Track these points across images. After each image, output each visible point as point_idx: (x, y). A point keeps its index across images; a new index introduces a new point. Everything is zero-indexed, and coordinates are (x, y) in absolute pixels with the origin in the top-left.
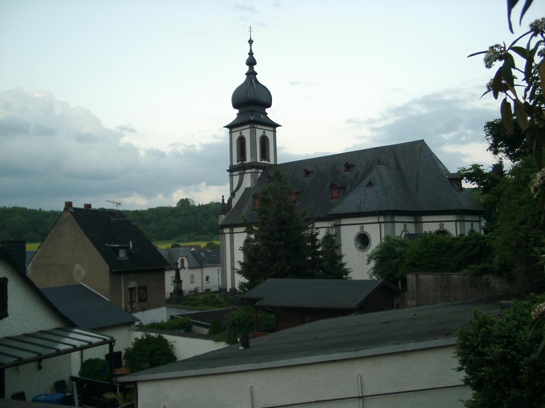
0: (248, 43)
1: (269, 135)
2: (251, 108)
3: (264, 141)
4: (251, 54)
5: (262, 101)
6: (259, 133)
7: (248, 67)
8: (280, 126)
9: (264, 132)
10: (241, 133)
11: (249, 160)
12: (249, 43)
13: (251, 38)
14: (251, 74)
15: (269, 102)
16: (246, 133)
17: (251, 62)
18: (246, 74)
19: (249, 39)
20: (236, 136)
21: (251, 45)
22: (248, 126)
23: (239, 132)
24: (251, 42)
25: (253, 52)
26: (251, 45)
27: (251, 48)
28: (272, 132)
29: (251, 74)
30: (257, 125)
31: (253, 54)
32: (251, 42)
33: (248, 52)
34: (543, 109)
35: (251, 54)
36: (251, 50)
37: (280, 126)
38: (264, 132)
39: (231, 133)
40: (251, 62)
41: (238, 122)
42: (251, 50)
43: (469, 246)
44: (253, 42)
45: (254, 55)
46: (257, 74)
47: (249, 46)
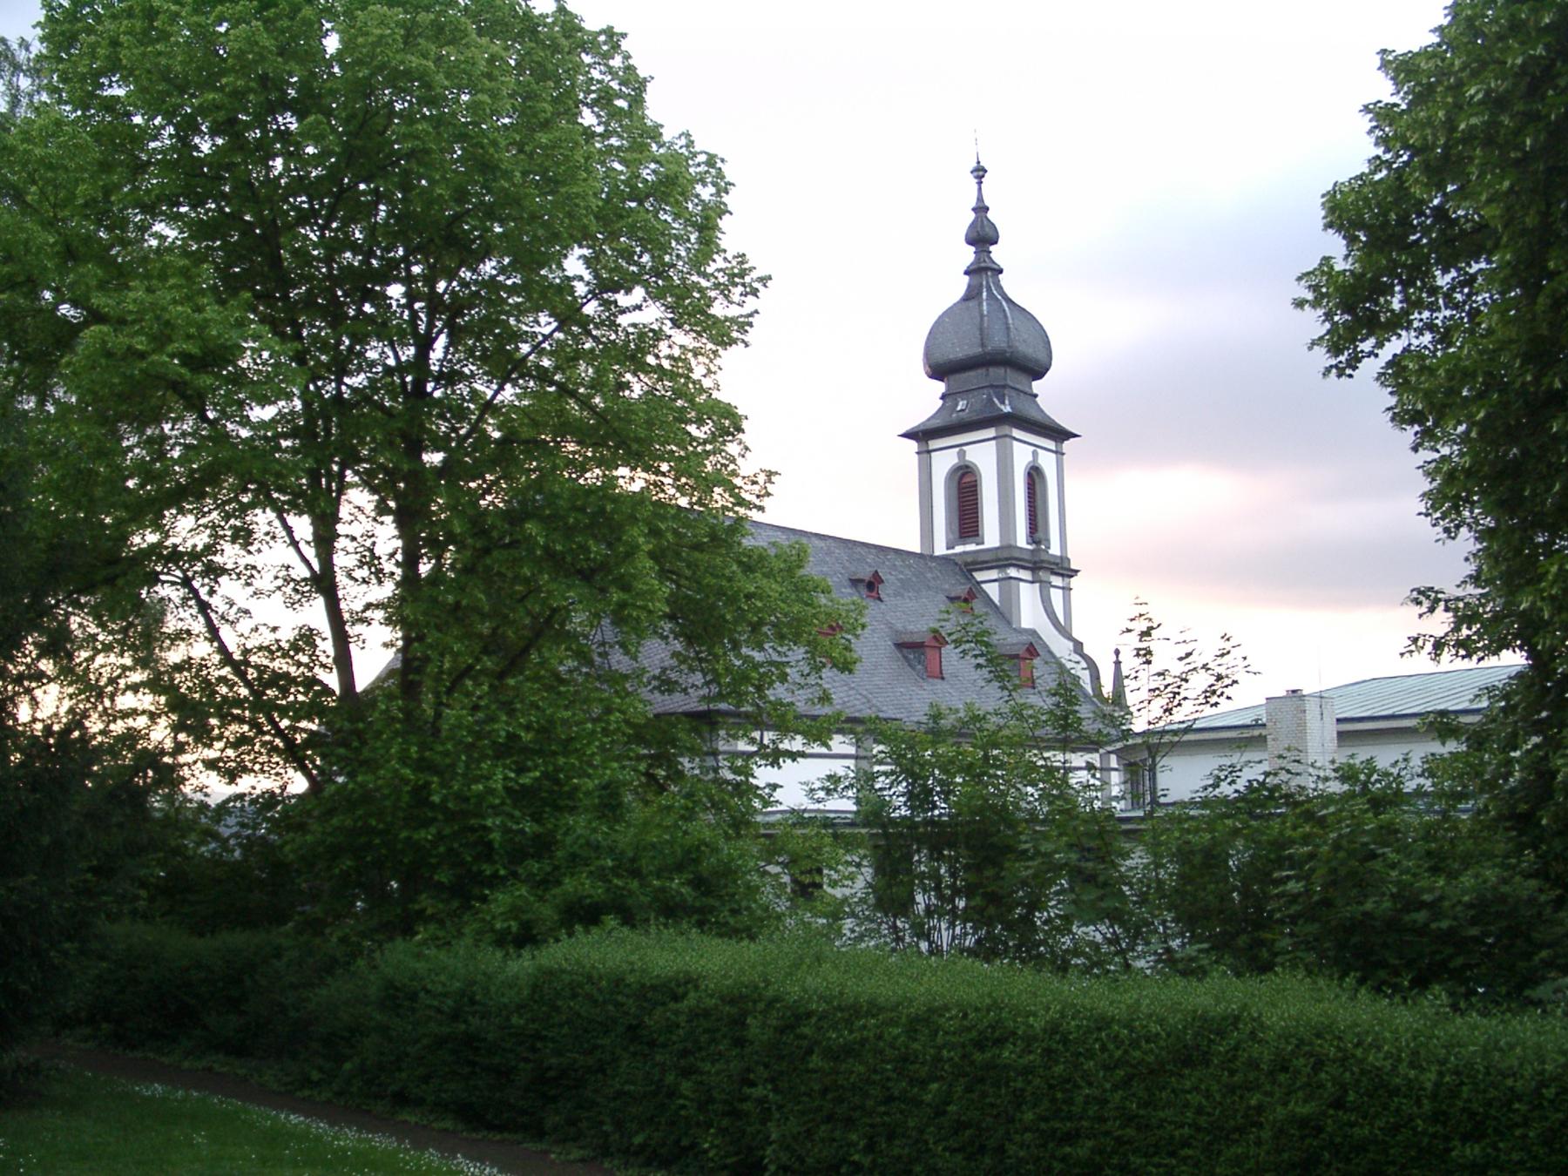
0: (971, 176)
1: (1047, 462)
2: (997, 373)
4: (981, 209)
5: (951, 357)
7: (973, 249)
8: (1076, 436)
9: (1035, 454)
10: (962, 454)
11: (991, 537)
12: (976, 177)
14: (983, 272)
15: (1041, 356)
16: (982, 453)
17: (982, 236)
18: (966, 273)
19: (974, 165)
20: (944, 462)
21: (980, 183)
22: (991, 432)
23: (957, 449)
24: (980, 172)
25: (987, 202)
26: (980, 183)
27: (980, 189)
28: (1054, 455)
29: (983, 272)
30: (930, 442)
31: (988, 209)
32: (980, 172)
33: (973, 203)
34: (316, 567)
35: (981, 209)
36: (980, 199)
37: (1076, 436)
38: (962, 454)
39: (924, 454)
40: (982, 236)
41: (938, 423)
42: (980, 199)
43: (1348, 1075)
45: (990, 215)
46: (1001, 271)
47: (976, 187)
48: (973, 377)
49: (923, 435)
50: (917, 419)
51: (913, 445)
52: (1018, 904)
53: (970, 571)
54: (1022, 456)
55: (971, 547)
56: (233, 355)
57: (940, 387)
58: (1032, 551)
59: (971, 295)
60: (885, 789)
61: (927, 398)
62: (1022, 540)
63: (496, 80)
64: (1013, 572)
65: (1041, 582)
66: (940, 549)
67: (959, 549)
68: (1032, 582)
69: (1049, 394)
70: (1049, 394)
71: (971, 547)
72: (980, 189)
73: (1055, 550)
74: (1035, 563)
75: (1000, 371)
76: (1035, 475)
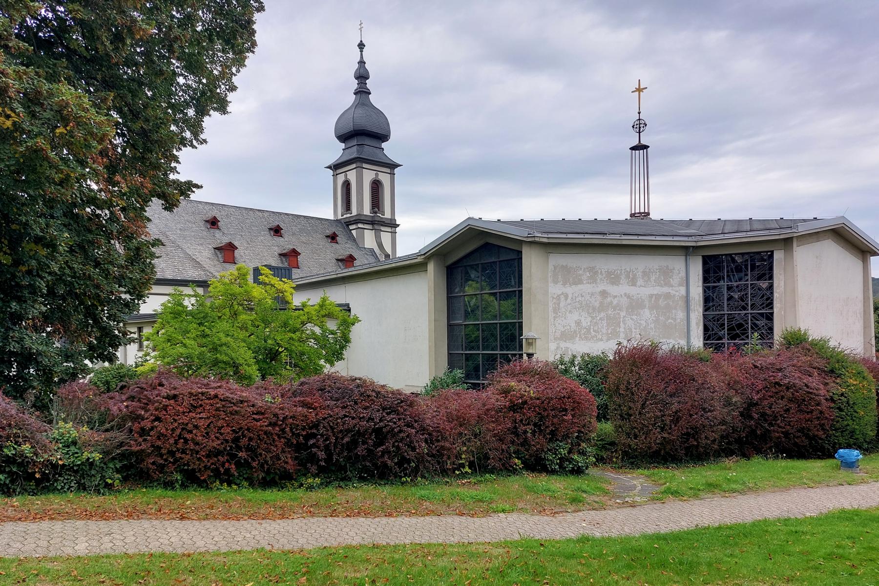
1: (385, 178)
3: (376, 186)
4: (362, 63)
6: (368, 176)
11: (354, 212)
13: (361, 41)
14: (362, 92)
17: (362, 76)
20: (341, 179)
21: (361, 51)
22: (354, 166)
24: (361, 46)
26: (361, 51)
27: (362, 55)
29: (362, 92)
32: (361, 46)
33: (358, 59)
35: (362, 63)
38: (377, 175)
40: (362, 76)
44: (365, 46)
46: (370, 93)
48: (354, 142)
49: (336, 167)
50: (333, 159)
51: (331, 172)
52: (321, 328)
53: (348, 226)
54: (368, 176)
55: (348, 215)
56: (750, 454)
57: (343, 145)
58: (372, 216)
59: (357, 105)
60: (18, 101)
61: (336, 151)
62: (367, 211)
63: (127, 399)
64: (360, 225)
65: (375, 229)
66: (340, 217)
67: (345, 216)
68: (372, 230)
69: (390, 149)
70: (390, 149)
71: (348, 215)
72: (362, 55)
73: (387, 215)
74: (372, 221)
75: (364, 137)
76: (376, 186)
